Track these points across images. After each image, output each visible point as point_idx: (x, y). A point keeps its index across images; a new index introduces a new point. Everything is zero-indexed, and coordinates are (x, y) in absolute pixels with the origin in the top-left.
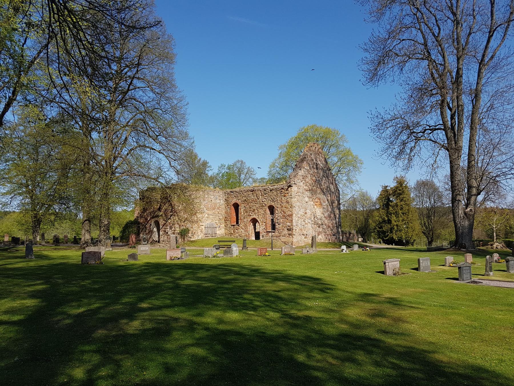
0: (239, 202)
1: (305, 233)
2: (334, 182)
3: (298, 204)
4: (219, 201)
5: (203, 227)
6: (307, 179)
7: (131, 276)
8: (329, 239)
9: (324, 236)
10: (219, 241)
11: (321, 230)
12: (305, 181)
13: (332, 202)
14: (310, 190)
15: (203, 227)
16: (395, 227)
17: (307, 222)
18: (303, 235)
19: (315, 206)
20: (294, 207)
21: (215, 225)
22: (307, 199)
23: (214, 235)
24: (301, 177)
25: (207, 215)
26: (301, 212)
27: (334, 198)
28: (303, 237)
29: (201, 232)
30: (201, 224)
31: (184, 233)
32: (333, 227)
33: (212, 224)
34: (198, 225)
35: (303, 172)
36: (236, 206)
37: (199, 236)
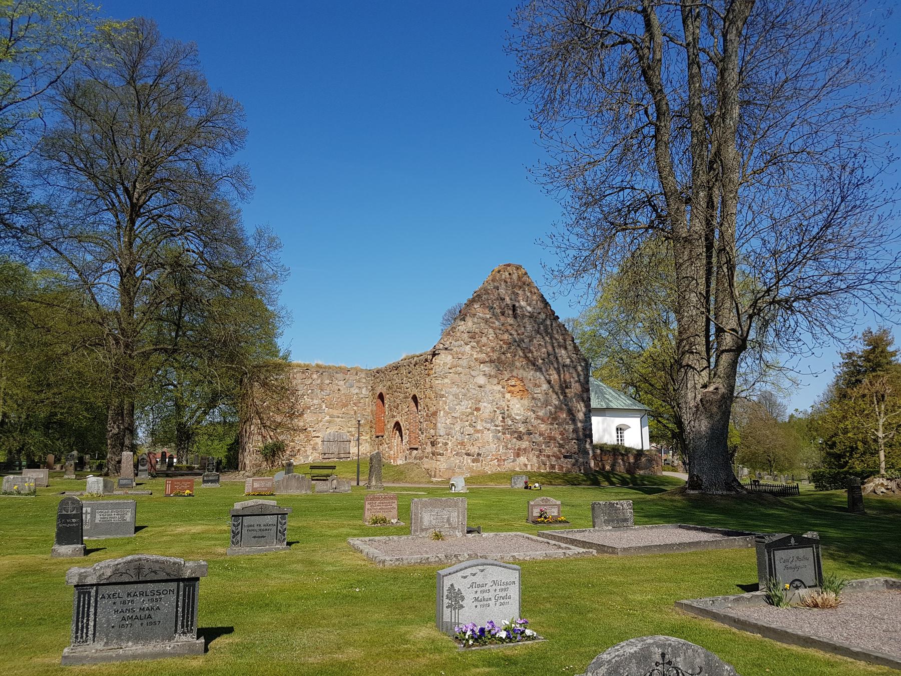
0: (384, 391)
1: (474, 450)
2: (569, 342)
3: (455, 389)
4: (357, 391)
5: (319, 441)
6: (484, 340)
7: (769, 556)
8: (553, 467)
9: (535, 459)
10: (312, 467)
11: (525, 444)
12: (478, 343)
13: (564, 386)
14: (491, 361)
15: (319, 441)
16: (860, 444)
17: (479, 427)
18: (468, 454)
19: (508, 396)
20: (442, 396)
21: (347, 436)
22: (481, 380)
23: (342, 456)
24: (466, 335)
25: (327, 418)
26: (465, 406)
27: (571, 378)
28: (469, 460)
29: (314, 449)
30: (314, 434)
31: (273, 452)
32: (567, 440)
33: (340, 435)
34: (307, 436)
35: (470, 324)
36: (381, 397)
37: (307, 457)
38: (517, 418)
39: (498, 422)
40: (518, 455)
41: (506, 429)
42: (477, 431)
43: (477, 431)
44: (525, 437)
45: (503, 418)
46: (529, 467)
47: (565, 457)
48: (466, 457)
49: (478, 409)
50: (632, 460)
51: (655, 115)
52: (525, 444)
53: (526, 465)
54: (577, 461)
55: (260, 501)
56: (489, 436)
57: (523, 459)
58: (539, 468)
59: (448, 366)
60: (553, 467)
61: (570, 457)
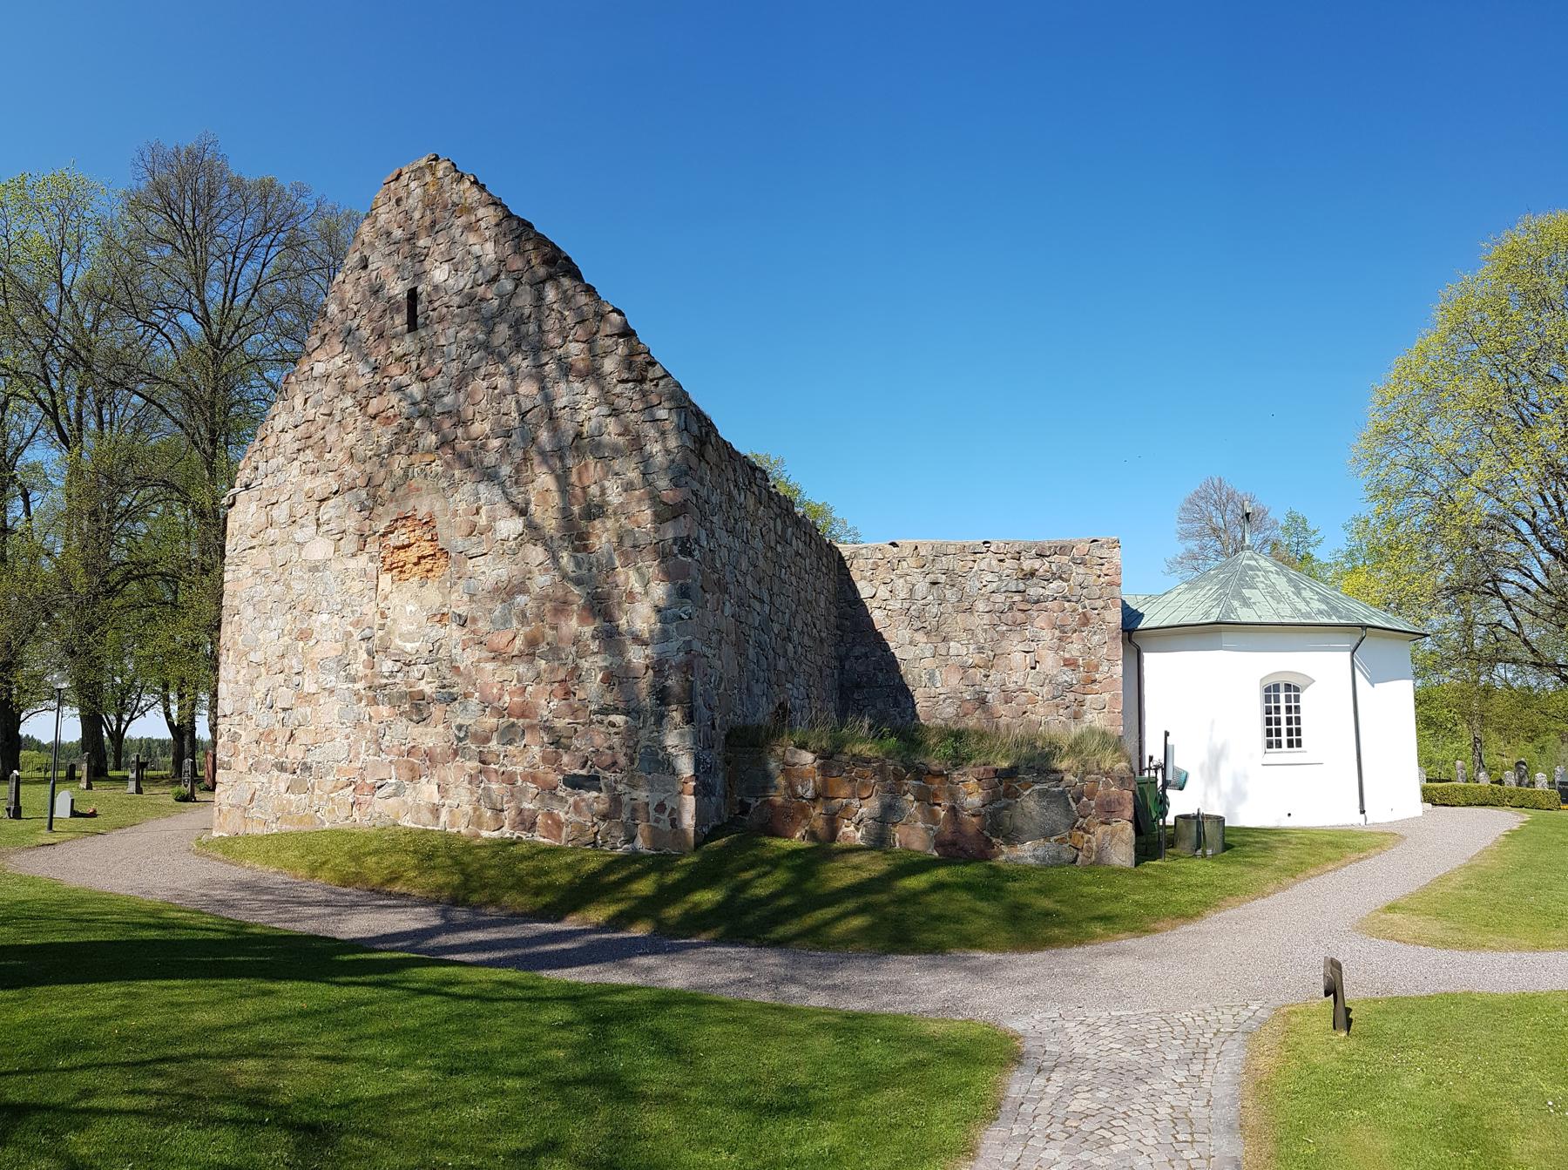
1: (295, 753)
11: (431, 737)
17: (309, 687)
18: (282, 768)
38: (409, 647)
39: (358, 668)
40: (415, 775)
41: (376, 692)
42: (308, 698)
43: (308, 698)
44: (436, 711)
45: (370, 653)
46: (444, 816)
47: (574, 783)
48: (276, 773)
49: (304, 635)
50: (973, 797)
51: (410, 1023)
52: (431, 737)
53: (435, 811)
54: (616, 800)
55: (558, 927)
56: (330, 711)
57: (428, 791)
58: (478, 821)
59: (250, 532)
60: (527, 822)
61: (590, 782)
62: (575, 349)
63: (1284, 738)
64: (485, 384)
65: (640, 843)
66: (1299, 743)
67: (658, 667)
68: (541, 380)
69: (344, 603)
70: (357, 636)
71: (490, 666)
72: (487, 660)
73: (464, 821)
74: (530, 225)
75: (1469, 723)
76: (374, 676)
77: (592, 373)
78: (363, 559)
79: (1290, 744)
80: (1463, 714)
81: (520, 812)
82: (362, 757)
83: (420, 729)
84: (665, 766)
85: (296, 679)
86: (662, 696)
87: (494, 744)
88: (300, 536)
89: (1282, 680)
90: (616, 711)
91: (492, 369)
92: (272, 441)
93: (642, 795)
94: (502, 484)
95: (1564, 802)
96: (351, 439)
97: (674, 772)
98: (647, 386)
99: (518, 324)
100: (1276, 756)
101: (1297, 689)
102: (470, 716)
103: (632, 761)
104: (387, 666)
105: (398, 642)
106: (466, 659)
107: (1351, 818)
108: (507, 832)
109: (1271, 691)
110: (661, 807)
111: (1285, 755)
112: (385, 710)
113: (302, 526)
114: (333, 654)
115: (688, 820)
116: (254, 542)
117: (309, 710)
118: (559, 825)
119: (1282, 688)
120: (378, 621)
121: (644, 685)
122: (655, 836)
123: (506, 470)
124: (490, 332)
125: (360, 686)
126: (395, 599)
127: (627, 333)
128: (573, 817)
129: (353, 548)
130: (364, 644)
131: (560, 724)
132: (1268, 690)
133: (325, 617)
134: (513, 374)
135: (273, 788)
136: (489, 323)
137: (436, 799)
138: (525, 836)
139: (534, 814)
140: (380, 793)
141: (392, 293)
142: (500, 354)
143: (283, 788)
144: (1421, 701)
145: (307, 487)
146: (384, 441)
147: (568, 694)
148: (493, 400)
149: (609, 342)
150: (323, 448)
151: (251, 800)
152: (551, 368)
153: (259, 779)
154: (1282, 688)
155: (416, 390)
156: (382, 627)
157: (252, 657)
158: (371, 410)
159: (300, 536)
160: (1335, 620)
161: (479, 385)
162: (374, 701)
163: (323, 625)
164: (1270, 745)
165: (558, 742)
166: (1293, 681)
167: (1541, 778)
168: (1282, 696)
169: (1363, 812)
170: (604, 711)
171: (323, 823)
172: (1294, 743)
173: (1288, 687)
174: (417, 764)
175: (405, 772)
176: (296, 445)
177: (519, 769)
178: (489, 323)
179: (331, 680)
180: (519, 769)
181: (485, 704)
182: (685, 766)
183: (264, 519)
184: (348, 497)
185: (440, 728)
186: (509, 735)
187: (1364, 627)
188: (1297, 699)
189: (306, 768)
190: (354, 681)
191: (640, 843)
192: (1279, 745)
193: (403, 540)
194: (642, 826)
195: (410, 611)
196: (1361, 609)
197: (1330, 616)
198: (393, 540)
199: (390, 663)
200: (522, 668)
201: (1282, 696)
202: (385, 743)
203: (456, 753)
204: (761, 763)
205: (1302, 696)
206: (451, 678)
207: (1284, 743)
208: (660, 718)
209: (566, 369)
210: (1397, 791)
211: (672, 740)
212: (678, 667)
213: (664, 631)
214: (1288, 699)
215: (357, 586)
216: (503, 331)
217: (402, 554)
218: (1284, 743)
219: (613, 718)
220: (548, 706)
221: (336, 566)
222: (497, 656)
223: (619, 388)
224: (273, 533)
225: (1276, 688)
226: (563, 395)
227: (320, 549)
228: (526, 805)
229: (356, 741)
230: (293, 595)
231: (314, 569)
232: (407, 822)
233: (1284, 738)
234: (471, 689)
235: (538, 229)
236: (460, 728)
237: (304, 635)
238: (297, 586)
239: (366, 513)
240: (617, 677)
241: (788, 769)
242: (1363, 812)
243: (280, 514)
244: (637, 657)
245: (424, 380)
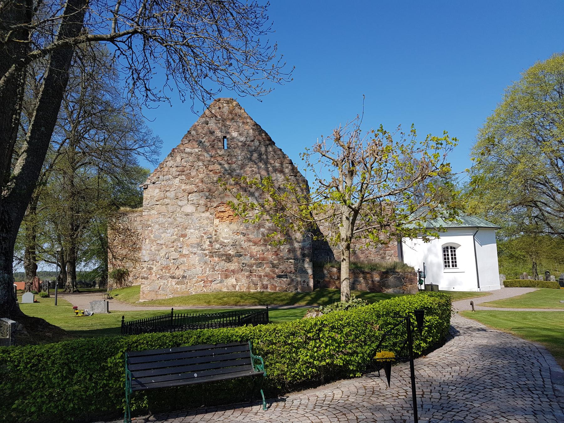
18: (173, 278)
38: (226, 241)
40: (227, 277)
42: (184, 256)
44: (235, 259)
46: (237, 288)
47: (280, 277)
48: (170, 279)
49: (184, 236)
52: (233, 266)
54: (292, 280)
56: (195, 259)
57: (232, 281)
58: (249, 288)
59: (155, 199)
61: (286, 276)
62: (277, 165)
63: (451, 264)
64: (250, 169)
65: (299, 290)
66: (456, 266)
67: (302, 249)
68: (268, 171)
69: (200, 227)
70: (205, 237)
71: (253, 247)
72: (252, 246)
73: (245, 288)
74: (274, 143)
75: (531, 256)
76: (212, 249)
77: (282, 172)
78: (207, 214)
79: (453, 266)
80: (527, 252)
81: (263, 285)
82: (207, 273)
83: (229, 264)
84: (305, 272)
85: (179, 250)
86: (304, 255)
87: (254, 268)
88: (180, 203)
89: (449, 246)
90: (291, 259)
91: (252, 166)
92: (166, 169)
93: (299, 279)
94: (256, 198)
95: (561, 286)
96: (201, 176)
97: (308, 273)
98: (297, 178)
99: (260, 155)
100: (447, 270)
101: (454, 248)
102: (247, 260)
103: (296, 271)
104: (217, 246)
105: (222, 239)
106: (245, 245)
107: (476, 289)
108: (259, 290)
109: (445, 249)
110: (304, 282)
111: (451, 269)
112: (216, 259)
113: (181, 200)
114: (196, 242)
115: (311, 284)
116: (158, 203)
117: (185, 259)
118: (276, 287)
119: (449, 248)
120: (214, 233)
121: (299, 253)
122: (302, 289)
123: (257, 194)
124: (252, 155)
125: (207, 252)
126: (220, 227)
127: (291, 163)
128: (281, 284)
129: (204, 209)
130: (208, 240)
131: (275, 262)
132: (444, 249)
133: (192, 231)
134: (259, 168)
135: (169, 284)
136: (251, 152)
137: (235, 283)
138: (265, 290)
139: (267, 285)
140: (215, 282)
141: (217, 135)
142: (255, 162)
143: (174, 283)
144: (498, 248)
145: (183, 188)
146: (215, 179)
147: (277, 255)
148: (251, 173)
149: (287, 165)
150: (188, 176)
151: (159, 288)
152: (271, 169)
153: (162, 282)
154: (449, 248)
155: (226, 166)
156: (216, 235)
157: (158, 242)
158: (210, 169)
159: (180, 203)
160: (467, 225)
161: (248, 169)
162: (212, 256)
163: (192, 233)
164: (446, 266)
165: (274, 266)
166: (453, 246)
167: (552, 277)
168: (449, 250)
169: (479, 287)
170: (288, 259)
171: (192, 293)
172: (455, 265)
173: (451, 248)
174: (227, 275)
175: (223, 276)
176: (178, 173)
177: (263, 274)
178: (251, 152)
179: (195, 250)
180: (263, 274)
181: (251, 257)
182: (310, 271)
183: (162, 195)
184: (201, 194)
185: (236, 264)
186: (260, 265)
187: (478, 227)
188: (455, 251)
189: (184, 277)
190: (204, 250)
191: (299, 290)
192: (449, 266)
193: (223, 209)
194: (300, 286)
195: (226, 231)
196: (477, 220)
197: (465, 224)
198: (219, 209)
199: (218, 245)
200: (263, 248)
201: (449, 250)
202: (217, 268)
203: (242, 270)
204: (322, 271)
205: (456, 251)
206: (240, 250)
207: (451, 266)
208: (304, 261)
209: (275, 170)
210: (492, 281)
211: (306, 266)
212: (308, 248)
213: (304, 239)
214: (451, 251)
215: (205, 222)
216: (255, 155)
217: (222, 214)
218: (451, 266)
219: (291, 261)
220: (271, 256)
221: (197, 215)
222: (255, 244)
223: (290, 177)
224: (167, 201)
225: (447, 248)
226: (274, 176)
227: (189, 209)
228: (265, 283)
229: (205, 268)
230: (177, 222)
231: (187, 215)
232: (225, 290)
233: (451, 264)
234: (247, 253)
235: (278, 145)
236: (243, 264)
237: (184, 236)
238: (179, 220)
239: (208, 200)
240: (292, 250)
241: (330, 272)
242: (479, 287)
243: (171, 194)
244: (296, 245)
245: (229, 164)
